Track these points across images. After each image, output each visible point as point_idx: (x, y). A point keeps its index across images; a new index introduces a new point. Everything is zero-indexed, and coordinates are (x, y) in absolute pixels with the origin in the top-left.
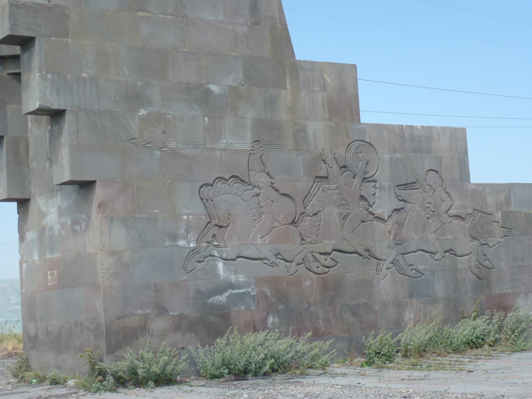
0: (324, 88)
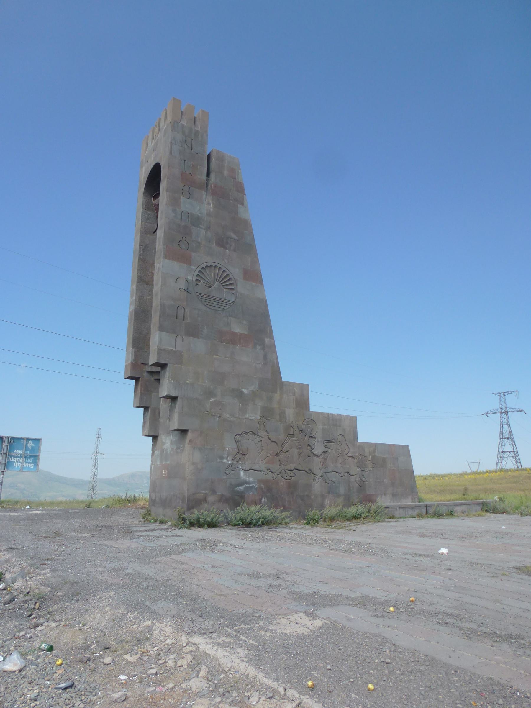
0: (294, 394)
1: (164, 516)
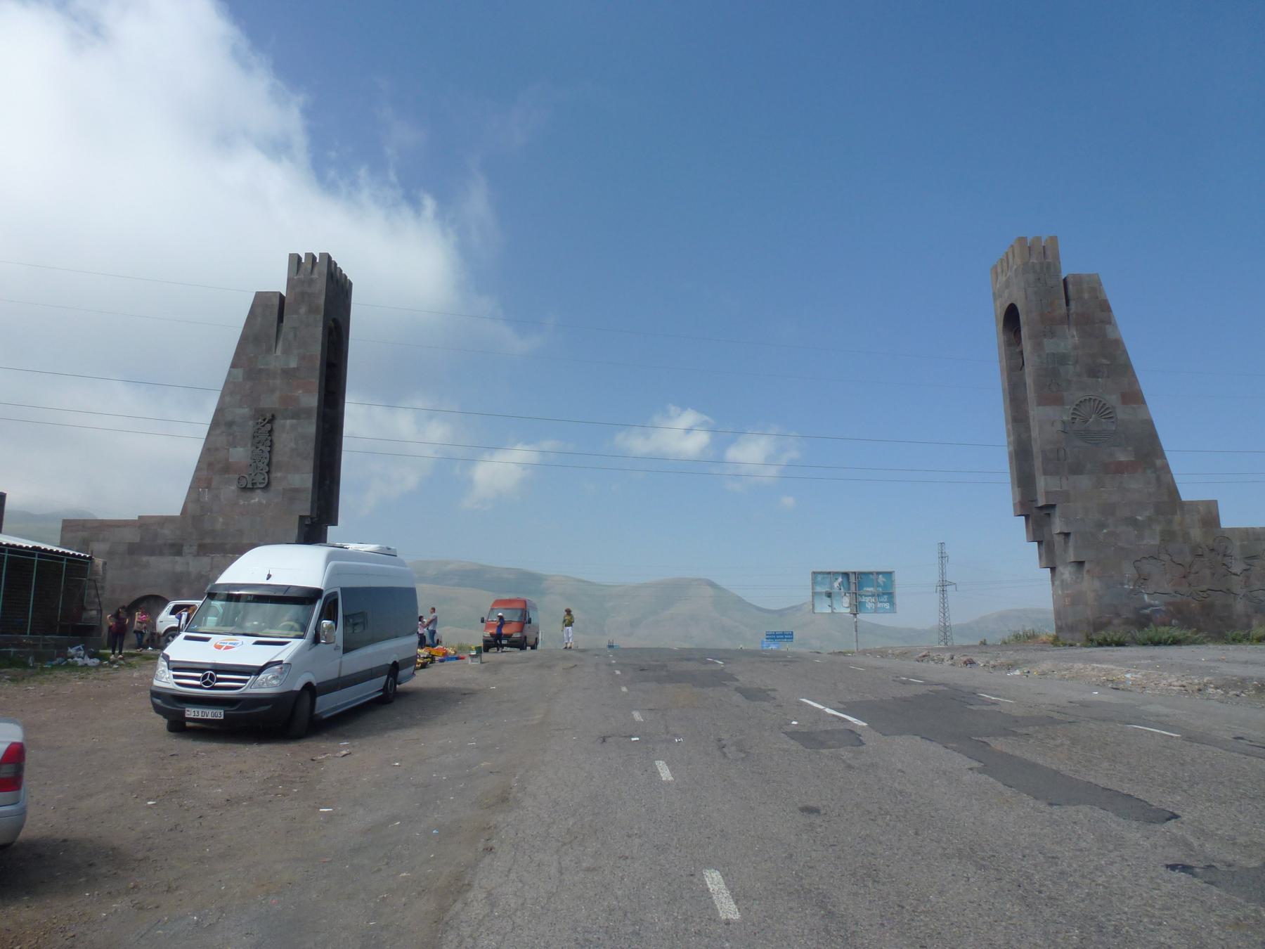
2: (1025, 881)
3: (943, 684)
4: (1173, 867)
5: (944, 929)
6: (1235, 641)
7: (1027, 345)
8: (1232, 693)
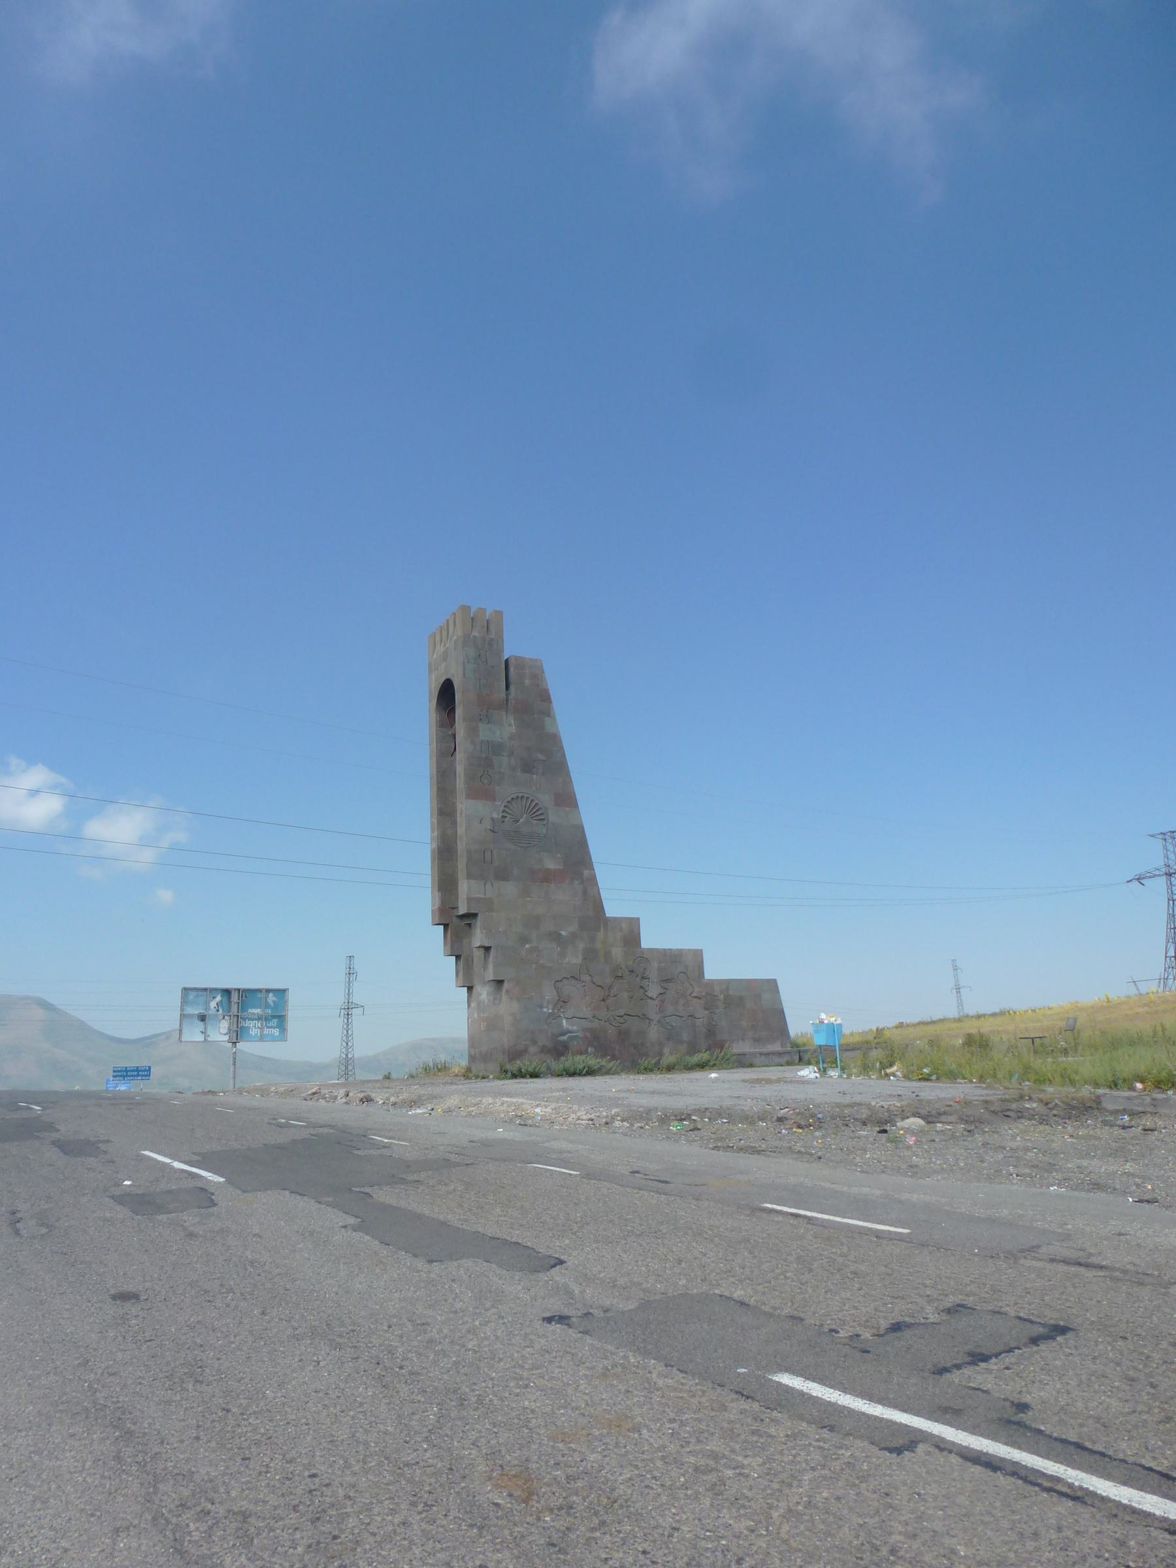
0: (621, 930)
1: (486, 1070)
2: (386, 1357)
3: (330, 1126)
4: (549, 1320)
5: (276, 1431)
6: (648, 1070)
7: (460, 728)
8: (636, 1125)
